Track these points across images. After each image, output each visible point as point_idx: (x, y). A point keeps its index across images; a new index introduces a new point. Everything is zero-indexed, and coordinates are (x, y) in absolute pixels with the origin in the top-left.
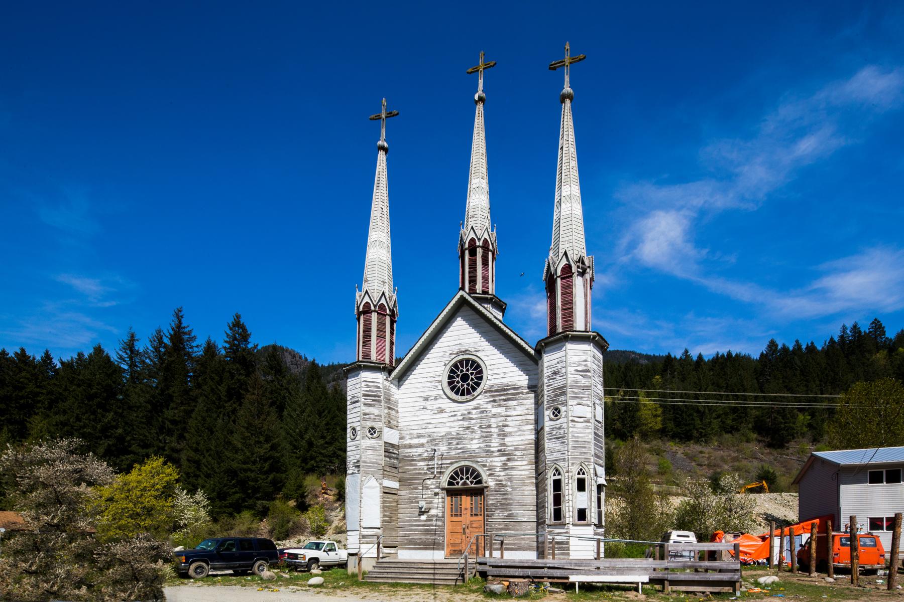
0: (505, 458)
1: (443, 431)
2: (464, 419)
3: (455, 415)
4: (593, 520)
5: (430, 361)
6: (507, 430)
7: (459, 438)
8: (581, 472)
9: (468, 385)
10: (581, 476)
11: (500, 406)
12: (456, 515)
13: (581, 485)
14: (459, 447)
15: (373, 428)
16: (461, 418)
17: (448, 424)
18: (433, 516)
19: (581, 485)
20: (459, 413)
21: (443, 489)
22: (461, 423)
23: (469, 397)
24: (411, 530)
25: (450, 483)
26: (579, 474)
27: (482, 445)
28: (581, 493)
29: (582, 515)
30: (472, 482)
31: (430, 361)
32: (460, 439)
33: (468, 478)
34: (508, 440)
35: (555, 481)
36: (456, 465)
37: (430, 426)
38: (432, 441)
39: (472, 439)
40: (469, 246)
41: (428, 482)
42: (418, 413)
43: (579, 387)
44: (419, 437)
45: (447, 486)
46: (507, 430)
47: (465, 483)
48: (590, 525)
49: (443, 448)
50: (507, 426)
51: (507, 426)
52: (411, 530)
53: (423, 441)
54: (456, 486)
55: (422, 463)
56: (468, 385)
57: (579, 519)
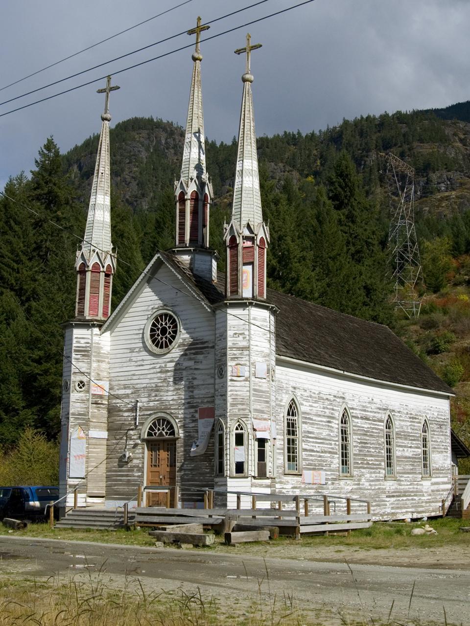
0: (192, 410)
1: (145, 382)
2: (160, 372)
3: (154, 368)
4: (250, 473)
5: (131, 315)
6: (196, 383)
7: (157, 389)
8: (240, 427)
9: (166, 338)
10: (239, 431)
11: (190, 359)
12: (155, 466)
13: (239, 440)
14: (157, 398)
15: (82, 382)
16: (159, 370)
17: (149, 376)
18: (134, 467)
19: (239, 440)
20: (158, 366)
21: (143, 440)
22: (159, 375)
23: (164, 350)
24: (116, 480)
25: (149, 434)
26: (237, 429)
27: (175, 397)
28: (239, 447)
29: (240, 468)
30: (166, 433)
31: (131, 315)
32: (157, 391)
33: (163, 429)
34: (196, 392)
35: (237, 435)
36: (154, 417)
37: (135, 377)
38: (136, 391)
39: (168, 391)
40: (179, 200)
41: (131, 432)
42: (125, 364)
43: (238, 349)
44: (125, 388)
45: (146, 437)
46: (196, 383)
47: (161, 434)
48: (247, 477)
49: (143, 401)
50: (195, 379)
51: (195, 379)
52: (116, 480)
53: (129, 391)
54: (154, 437)
55: (126, 414)
56: (166, 338)
57: (237, 472)
